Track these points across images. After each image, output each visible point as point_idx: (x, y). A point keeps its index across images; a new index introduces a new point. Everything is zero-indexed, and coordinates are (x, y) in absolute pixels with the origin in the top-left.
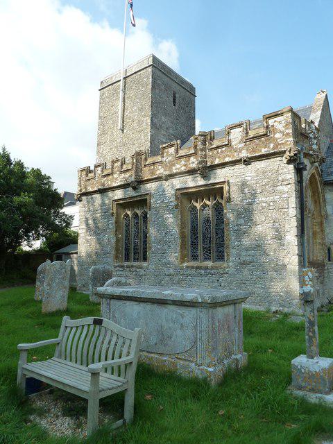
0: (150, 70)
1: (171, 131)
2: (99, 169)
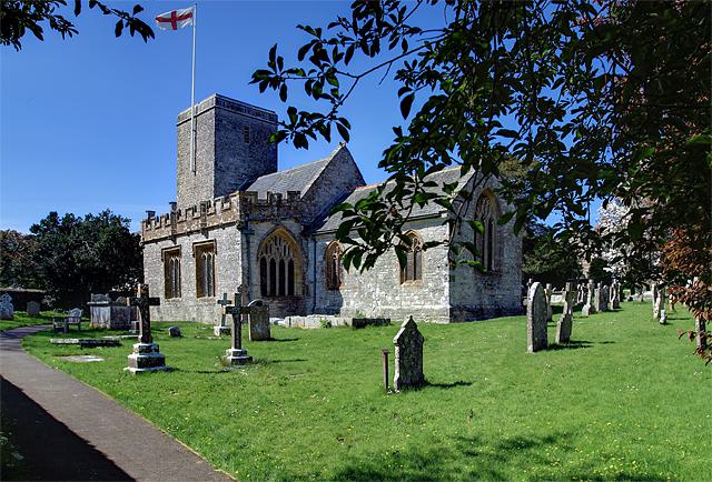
0: (213, 111)
1: (242, 170)
2: (191, 212)
